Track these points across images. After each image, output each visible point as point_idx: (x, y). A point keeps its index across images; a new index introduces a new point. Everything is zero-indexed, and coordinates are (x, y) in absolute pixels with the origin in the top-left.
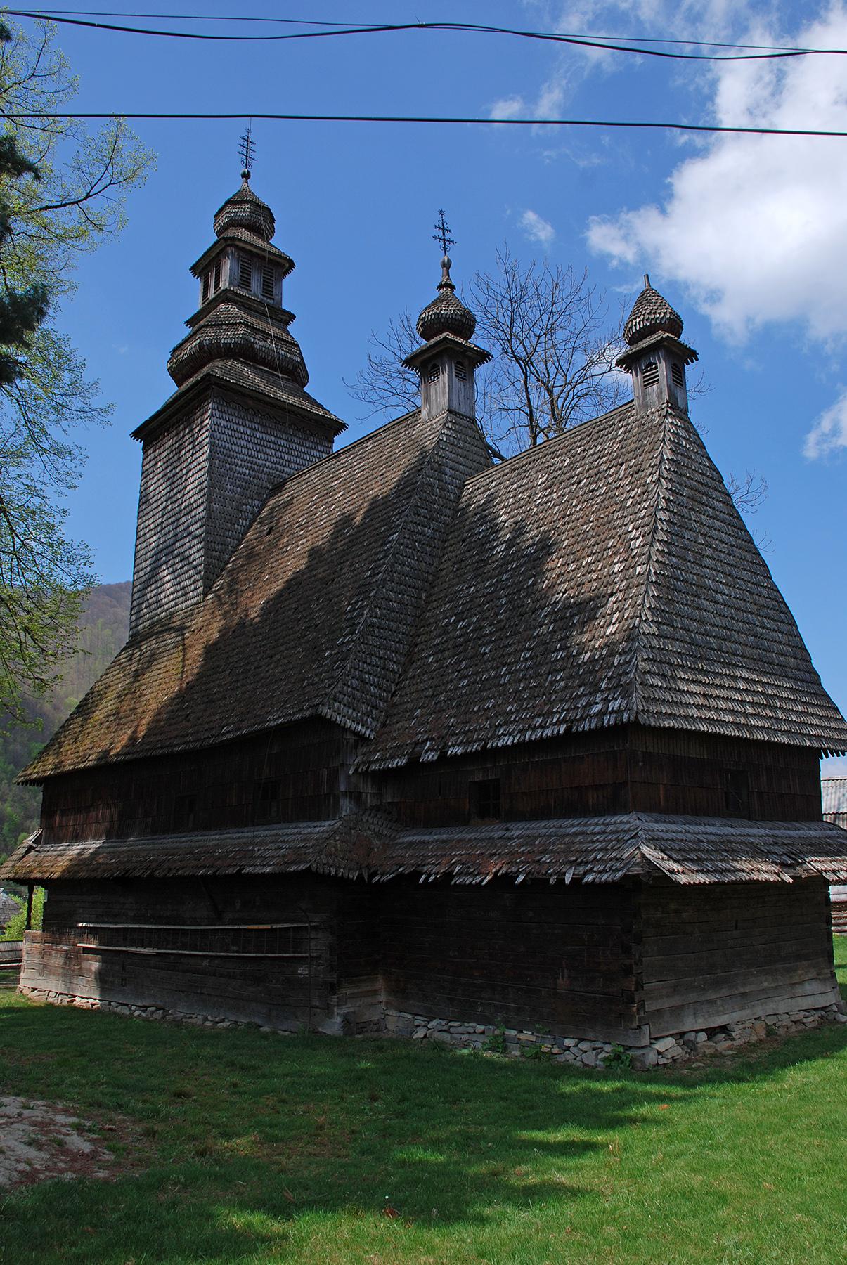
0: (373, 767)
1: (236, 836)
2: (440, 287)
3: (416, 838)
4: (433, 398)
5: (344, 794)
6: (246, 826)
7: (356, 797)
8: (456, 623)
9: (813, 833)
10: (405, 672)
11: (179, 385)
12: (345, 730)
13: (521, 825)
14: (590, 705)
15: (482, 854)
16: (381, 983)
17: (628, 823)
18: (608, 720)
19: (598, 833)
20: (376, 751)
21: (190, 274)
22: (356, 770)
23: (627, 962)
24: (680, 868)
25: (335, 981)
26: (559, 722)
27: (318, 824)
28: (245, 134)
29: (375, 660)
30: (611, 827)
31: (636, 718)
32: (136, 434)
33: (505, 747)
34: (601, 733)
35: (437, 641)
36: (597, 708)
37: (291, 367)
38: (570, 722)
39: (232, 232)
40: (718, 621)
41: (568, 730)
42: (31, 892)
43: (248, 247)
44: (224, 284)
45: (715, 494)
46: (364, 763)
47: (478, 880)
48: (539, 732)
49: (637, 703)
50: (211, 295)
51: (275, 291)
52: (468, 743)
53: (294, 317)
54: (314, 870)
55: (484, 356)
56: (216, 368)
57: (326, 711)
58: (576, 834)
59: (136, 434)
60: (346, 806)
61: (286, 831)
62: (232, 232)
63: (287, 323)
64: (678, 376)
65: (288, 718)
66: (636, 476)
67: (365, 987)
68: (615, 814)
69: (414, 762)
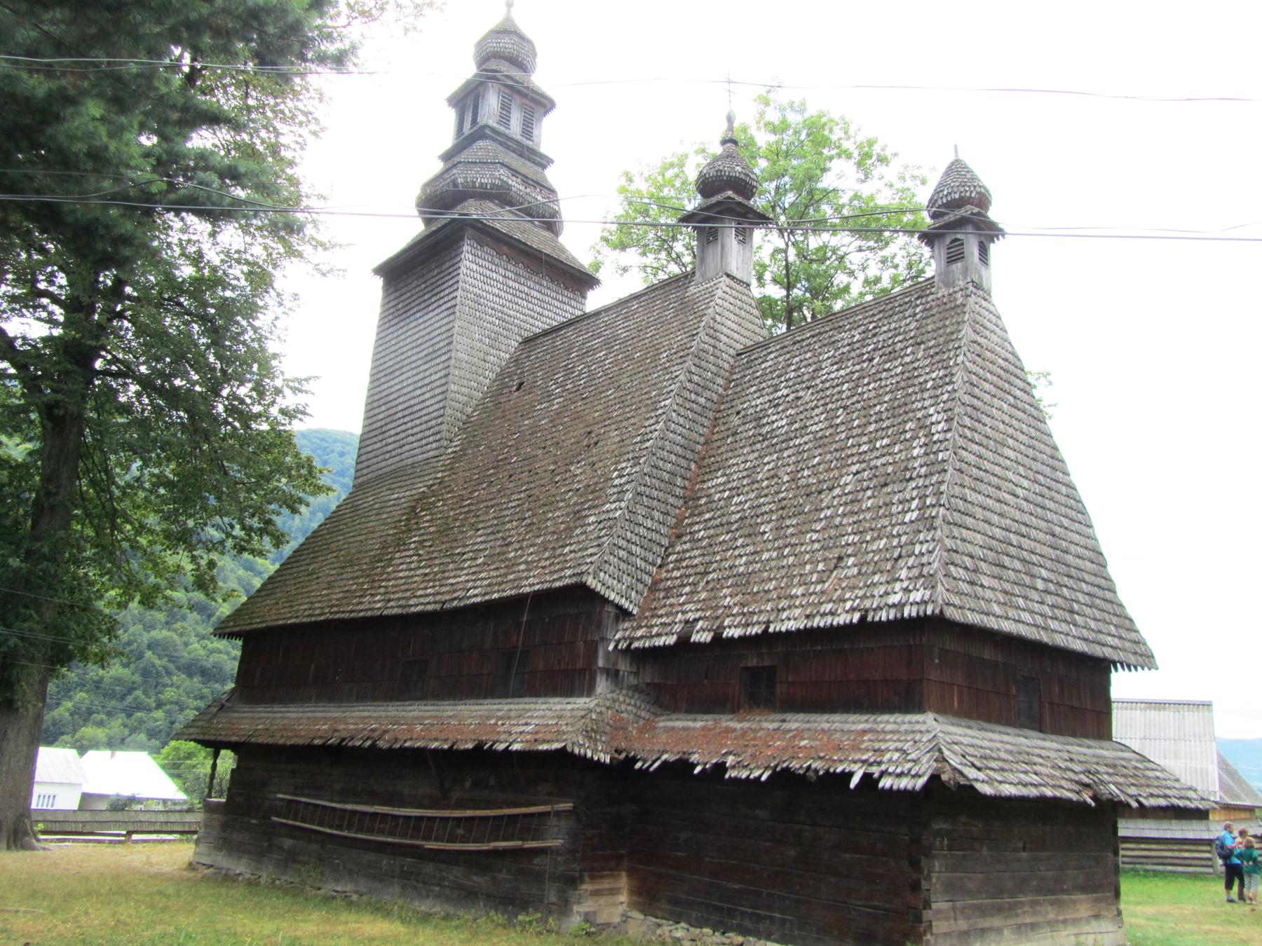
0: (636, 645)
1: (473, 708)
6: (486, 697)
7: (613, 674)
10: (672, 545)
12: (605, 601)
14: (887, 593)
16: (623, 881)
17: (924, 723)
19: (891, 732)
20: (640, 627)
22: (616, 646)
23: (915, 876)
25: (577, 874)
26: (853, 609)
30: (903, 728)
31: (941, 611)
32: (380, 271)
34: (902, 626)
39: (493, 65)
40: (1018, 515)
41: (863, 619)
42: (216, 755)
44: (482, 120)
45: (1017, 382)
46: (625, 639)
47: (756, 774)
49: (941, 592)
50: (467, 129)
51: (535, 132)
53: (552, 162)
54: (569, 750)
56: (474, 210)
57: (591, 582)
58: (864, 732)
60: (602, 685)
61: (533, 706)
62: (493, 65)
65: (546, 586)
66: (937, 358)
67: (606, 884)
68: (906, 710)
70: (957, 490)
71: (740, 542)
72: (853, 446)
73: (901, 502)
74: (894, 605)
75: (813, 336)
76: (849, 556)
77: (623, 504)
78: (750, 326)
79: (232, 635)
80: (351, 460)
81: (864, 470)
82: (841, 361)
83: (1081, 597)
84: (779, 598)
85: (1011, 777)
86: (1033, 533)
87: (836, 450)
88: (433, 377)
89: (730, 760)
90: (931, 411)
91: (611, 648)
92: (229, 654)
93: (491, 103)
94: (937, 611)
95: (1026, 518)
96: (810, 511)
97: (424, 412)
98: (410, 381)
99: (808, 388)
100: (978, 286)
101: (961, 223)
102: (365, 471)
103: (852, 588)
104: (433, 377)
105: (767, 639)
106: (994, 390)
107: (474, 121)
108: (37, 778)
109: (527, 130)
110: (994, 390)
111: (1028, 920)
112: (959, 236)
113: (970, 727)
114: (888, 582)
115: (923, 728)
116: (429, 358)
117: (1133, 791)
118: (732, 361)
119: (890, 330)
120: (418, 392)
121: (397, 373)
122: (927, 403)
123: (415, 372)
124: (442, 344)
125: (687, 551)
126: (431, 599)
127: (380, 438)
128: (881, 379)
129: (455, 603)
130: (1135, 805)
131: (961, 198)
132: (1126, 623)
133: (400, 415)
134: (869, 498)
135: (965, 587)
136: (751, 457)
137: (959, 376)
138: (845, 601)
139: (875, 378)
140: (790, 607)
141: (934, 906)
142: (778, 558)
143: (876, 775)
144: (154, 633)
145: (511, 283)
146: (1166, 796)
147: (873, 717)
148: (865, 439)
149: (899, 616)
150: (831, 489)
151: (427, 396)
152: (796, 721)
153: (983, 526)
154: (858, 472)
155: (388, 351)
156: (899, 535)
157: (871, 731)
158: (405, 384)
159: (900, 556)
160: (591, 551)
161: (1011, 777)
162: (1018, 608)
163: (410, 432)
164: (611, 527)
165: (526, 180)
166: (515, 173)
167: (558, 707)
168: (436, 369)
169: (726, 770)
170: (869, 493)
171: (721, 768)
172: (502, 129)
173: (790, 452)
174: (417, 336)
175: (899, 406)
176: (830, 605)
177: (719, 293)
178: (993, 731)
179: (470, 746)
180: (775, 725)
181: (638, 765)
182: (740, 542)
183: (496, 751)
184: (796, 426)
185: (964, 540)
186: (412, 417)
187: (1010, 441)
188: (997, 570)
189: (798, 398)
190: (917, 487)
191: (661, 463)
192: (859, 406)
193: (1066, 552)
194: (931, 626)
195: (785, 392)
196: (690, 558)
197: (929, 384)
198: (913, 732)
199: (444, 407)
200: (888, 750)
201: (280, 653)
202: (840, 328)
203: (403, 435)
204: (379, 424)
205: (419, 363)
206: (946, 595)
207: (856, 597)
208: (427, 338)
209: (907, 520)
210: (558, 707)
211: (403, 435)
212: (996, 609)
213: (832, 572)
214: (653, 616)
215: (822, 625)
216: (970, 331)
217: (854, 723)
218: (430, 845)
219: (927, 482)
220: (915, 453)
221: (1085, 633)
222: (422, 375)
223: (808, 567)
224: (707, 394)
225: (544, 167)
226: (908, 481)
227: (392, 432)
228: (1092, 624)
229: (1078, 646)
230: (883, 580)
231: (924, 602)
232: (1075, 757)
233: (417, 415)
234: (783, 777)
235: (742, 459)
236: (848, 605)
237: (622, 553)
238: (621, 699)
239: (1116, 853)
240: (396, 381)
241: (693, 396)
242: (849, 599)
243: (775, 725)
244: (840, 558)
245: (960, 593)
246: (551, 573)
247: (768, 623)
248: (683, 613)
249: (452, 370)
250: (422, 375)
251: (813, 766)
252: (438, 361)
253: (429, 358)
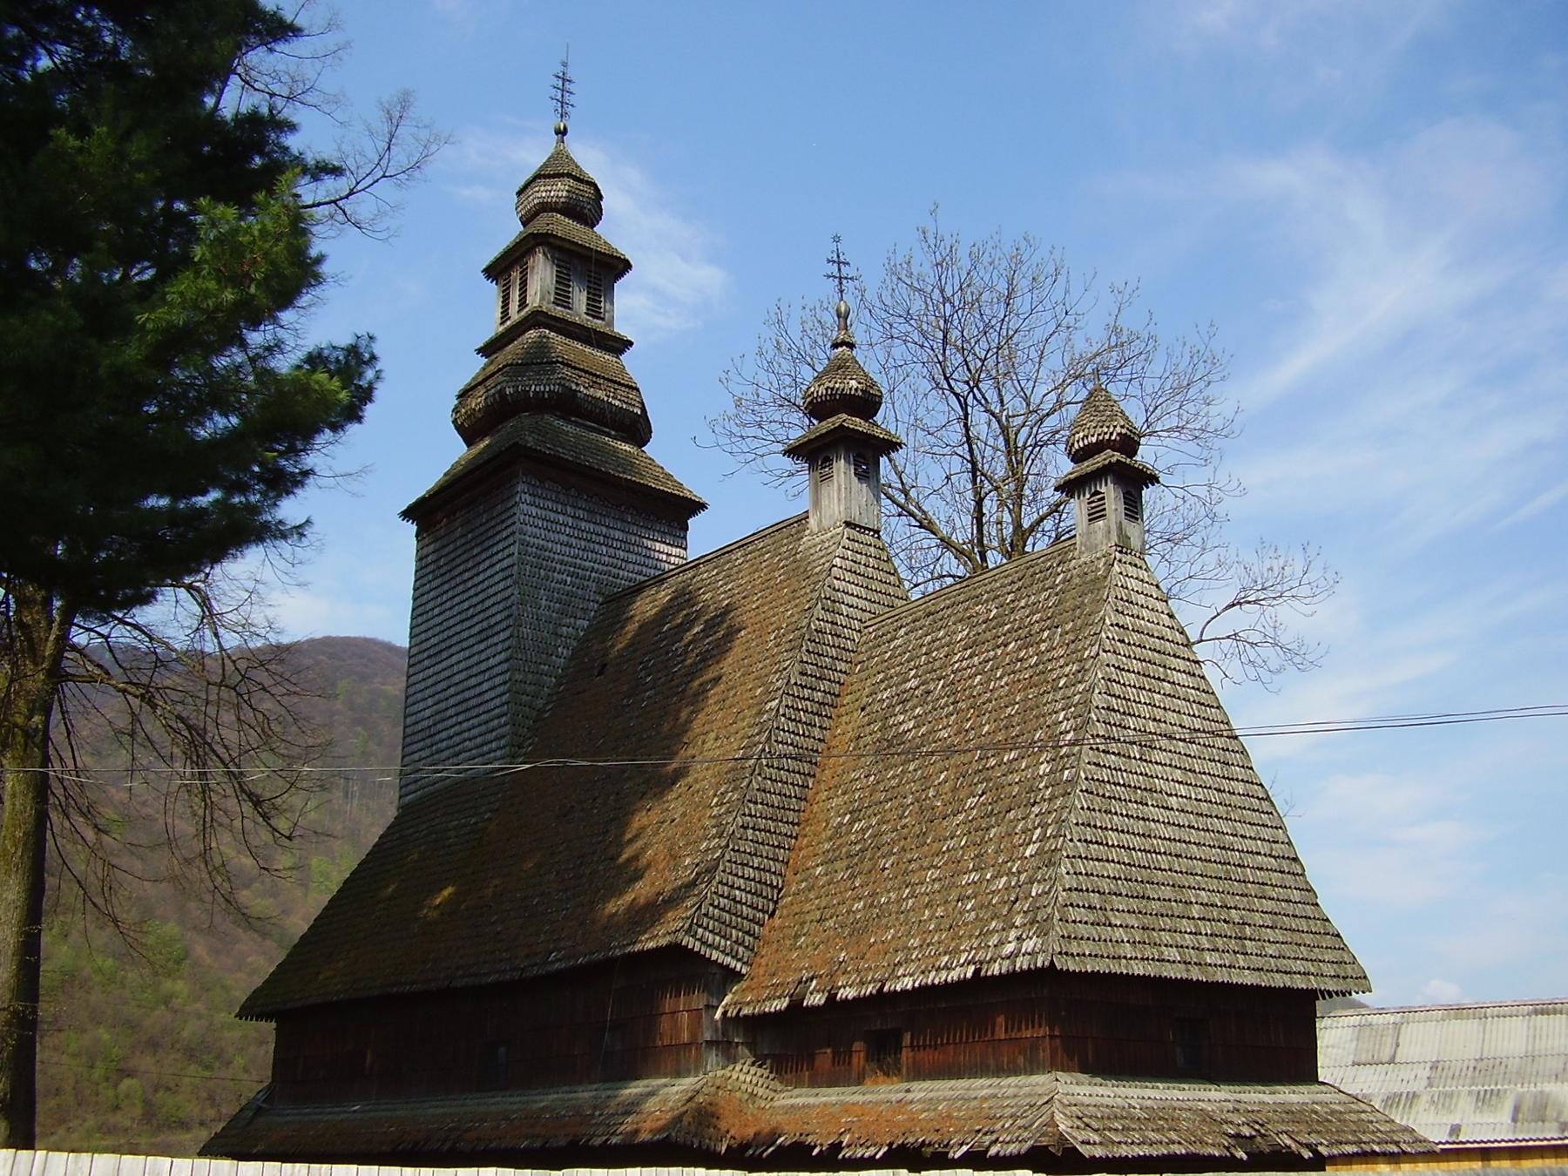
0: (746, 1011)
2: (835, 346)
4: (825, 502)
5: (710, 1043)
6: (580, 1083)
8: (852, 823)
9: (1294, 1098)
11: (469, 442)
13: (927, 1084)
14: (1001, 943)
18: (1022, 963)
22: (725, 1013)
24: (1097, 1139)
28: (559, 70)
29: (749, 872)
32: (408, 514)
33: (904, 992)
35: (827, 846)
36: (1009, 948)
37: (627, 421)
41: (977, 971)
43: (567, 246)
44: (534, 301)
47: (872, 1151)
48: (943, 975)
50: (515, 315)
52: (862, 983)
55: (891, 446)
59: (408, 514)
63: (622, 352)
64: (1133, 508)
66: (1072, 646)
69: (796, 1004)
78: (883, 587)
80: (395, 687)
88: (492, 662)
89: (846, 1139)
91: (718, 1015)
97: (482, 709)
98: (462, 666)
102: (412, 787)
104: (492, 662)
107: (523, 304)
109: (594, 310)
116: (484, 635)
117: (1313, 1139)
120: (473, 681)
121: (444, 655)
123: (467, 653)
124: (498, 618)
127: (428, 741)
130: (1307, 1154)
133: (451, 712)
145: (583, 525)
151: (485, 686)
155: (432, 623)
158: (455, 669)
163: (466, 735)
168: (492, 651)
172: (559, 311)
174: (466, 605)
179: (563, 1142)
183: (593, 1147)
186: (468, 715)
192: (990, 706)
203: (457, 739)
204: (425, 723)
205: (472, 641)
208: (479, 608)
211: (457, 739)
212: (1128, 950)
221: (1259, 962)
222: (475, 659)
227: (444, 735)
229: (1249, 979)
233: (474, 712)
240: (444, 665)
250: (475, 659)
252: (495, 639)
253: (484, 635)
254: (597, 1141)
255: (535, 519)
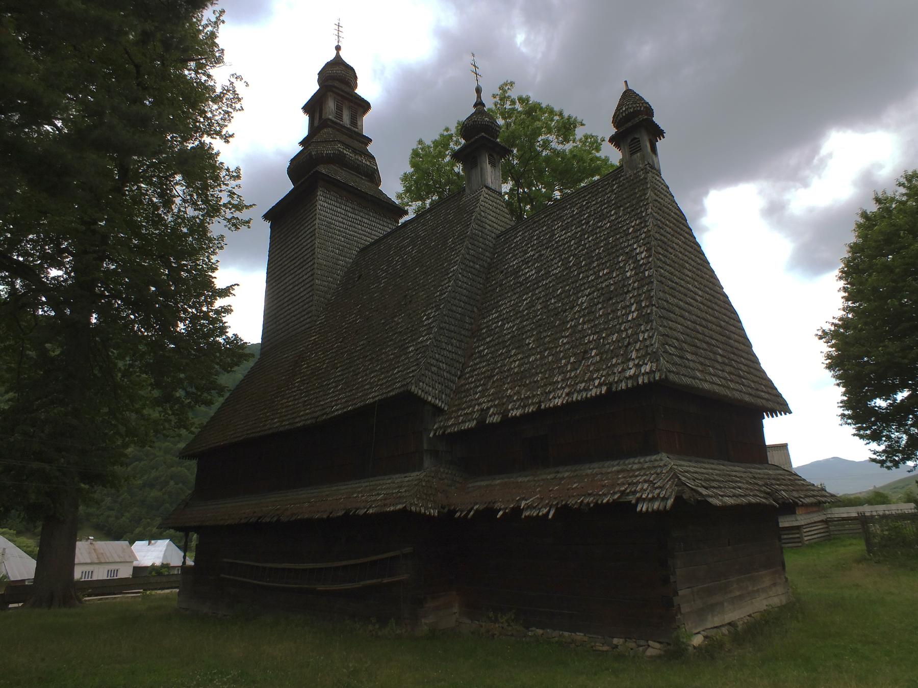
3: (484, 483)
12: (426, 402)
14: (624, 370)
15: (533, 494)
17: (661, 460)
21: (301, 111)
22: (435, 434)
26: (600, 385)
27: (407, 474)
30: (646, 466)
32: (267, 217)
36: (632, 372)
38: (610, 385)
39: (330, 83)
41: (609, 390)
42: (187, 536)
46: (440, 428)
51: (359, 123)
57: (413, 388)
58: (618, 472)
60: (427, 462)
61: (381, 482)
65: (385, 396)
68: (646, 455)
70: (661, 294)
71: (513, 352)
72: (583, 278)
73: (623, 308)
74: (630, 377)
75: (546, 217)
76: (592, 349)
77: (431, 336)
78: (504, 219)
79: (191, 457)
81: (594, 292)
82: (567, 228)
83: (742, 367)
84: (545, 385)
85: (728, 492)
86: (710, 325)
87: (573, 283)
90: (635, 246)
91: (431, 435)
92: (189, 470)
93: (331, 105)
94: (663, 376)
95: (704, 315)
96: (559, 325)
99: (547, 248)
100: (653, 167)
101: (636, 128)
103: (598, 371)
105: (541, 414)
106: (672, 233)
108: (76, 561)
110: (672, 233)
111: (738, 593)
112: (637, 136)
113: (690, 461)
114: (623, 363)
115: (662, 464)
118: (494, 241)
119: (597, 203)
120: (296, 288)
122: (631, 242)
125: (477, 364)
126: (309, 416)
128: (596, 233)
129: (324, 417)
131: (634, 111)
132: (769, 386)
134: (600, 309)
135: (677, 359)
136: (514, 297)
137: (650, 221)
138: (594, 379)
139: (591, 233)
140: (554, 390)
141: (680, 593)
142: (541, 358)
143: (633, 502)
144: (173, 469)
146: (813, 496)
147: (622, 462)
148: (591, 272)
149: (635, 384)
150: (572, 308)
152: (567, 471)
153: (680, 320)
154: (590, 294)
156: (626, 330)
157: (622, 471)
159: (629, 344)
160: (413, 368)
161: (728, 492)
162: (710, 374)
164: (425, 352)
165: (355, 151)
166: (347, 146)
167: (399, 480)
169: (521, 511)
170: (600, 306)
171: (517, 511)
173: (540, 289)
175: (612, 248)
176: (583, 385)
177: (482, 198)
178: (704, 463)
179: (341, 513)
180: (552, 476)
181: (458, 514)
182: (513, 352)
184: (543, 272)
185: (671, 328)
187: (687, 265)
188: (693, 349)
189: (541, 255)
190: (633, 296)
191: (454, 308)
193: (730, 338)
194: (660, 389)
195: (532, 253)
196: (480, 368)
197: (631, 230)
198: (655, 467)
199: (312, 295)
200: (638, 483)
201: (224, 465)
202: (565, 208)
206: (668, 365)
207: (602, 376)
209: (630, 318)
210: (399, 480)
213: (581, 362)
214: (458, 410)
215: (579, 398)
216: (652, 194)
217: (609, 467)
218: (320, 588)
219: (640, 292)
220: (628, 274)
223: (563, 361)
224: (481, 263)
225: (367, 145)
226: (626, 293)
228: (753, 385)
230: (619, 361)
231: (652, 372)
232: (756, 476)
234: (564, 511)
235: (508, 299)
236: (597, 382)
237: (434, 369)
238: (442, 470)
239: (780, 539)
241: (472, 264)
242: (597, 378)
243: (552, 476)
244: (585, 352)
245: (675, 364)
246: (387, 387)
247: (540, 402)
248: (479, 404)
249: (316, 271)
251: (586, 501)
254: (362, 512)
255: (326, 208)
